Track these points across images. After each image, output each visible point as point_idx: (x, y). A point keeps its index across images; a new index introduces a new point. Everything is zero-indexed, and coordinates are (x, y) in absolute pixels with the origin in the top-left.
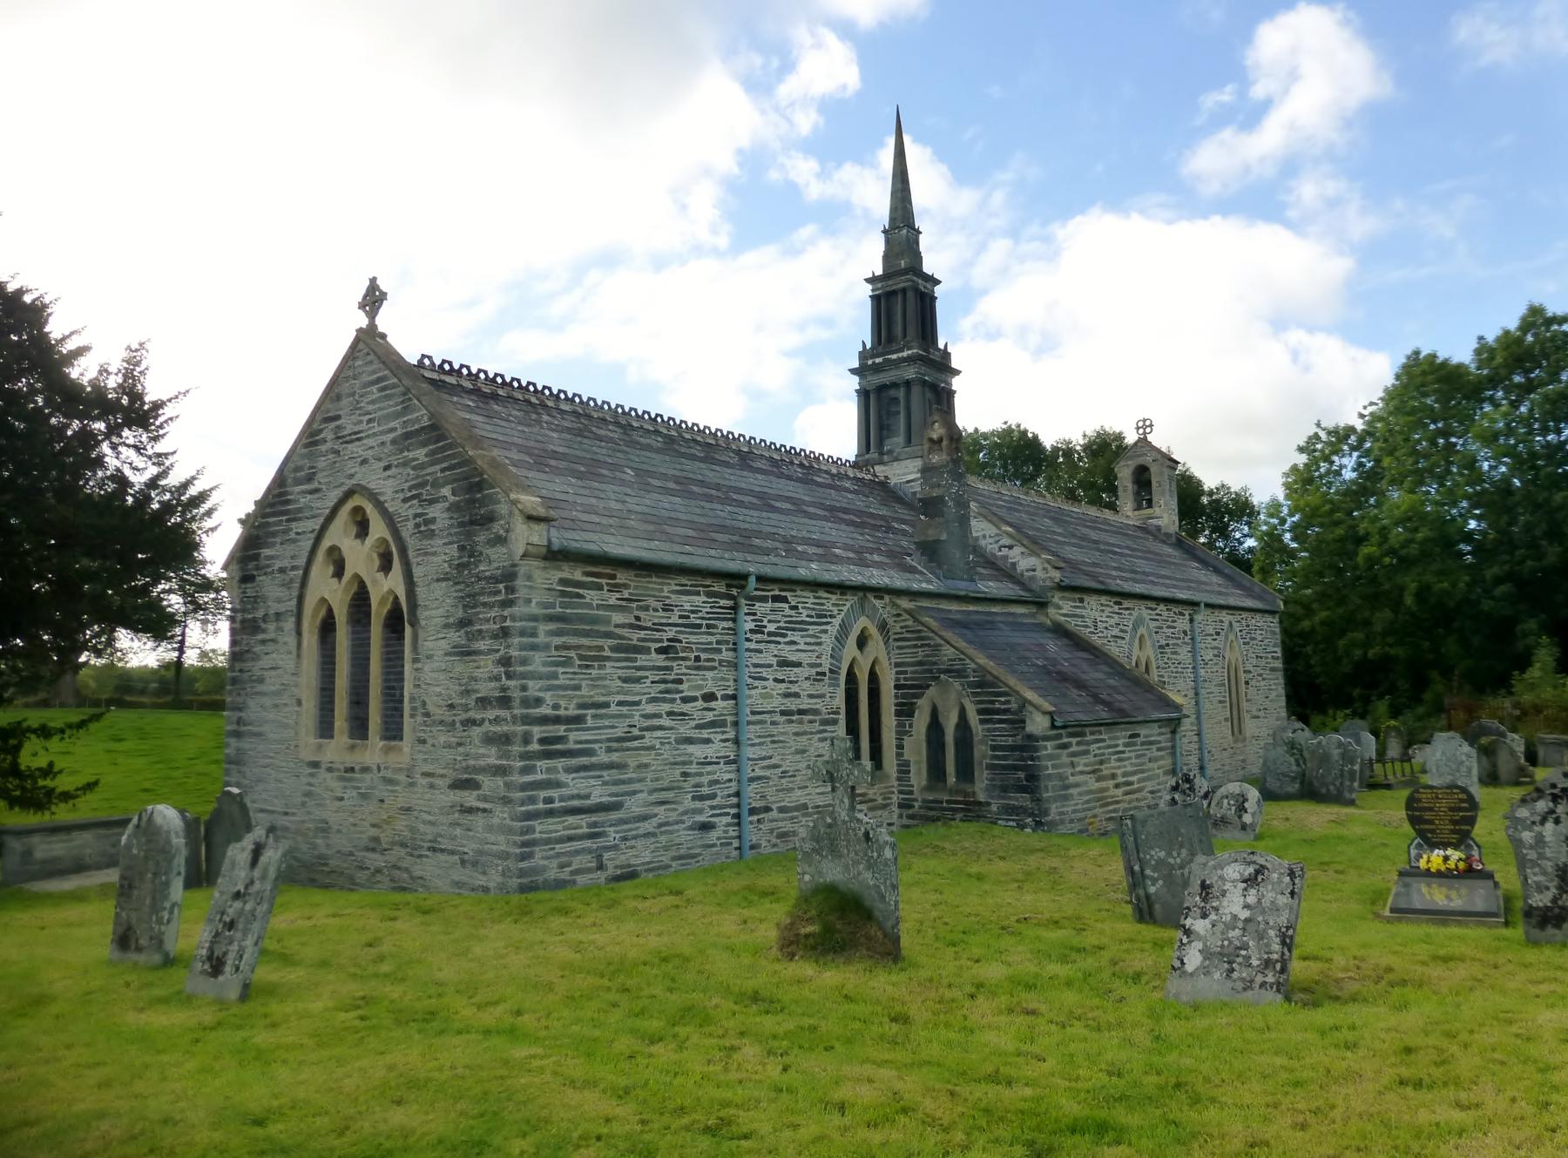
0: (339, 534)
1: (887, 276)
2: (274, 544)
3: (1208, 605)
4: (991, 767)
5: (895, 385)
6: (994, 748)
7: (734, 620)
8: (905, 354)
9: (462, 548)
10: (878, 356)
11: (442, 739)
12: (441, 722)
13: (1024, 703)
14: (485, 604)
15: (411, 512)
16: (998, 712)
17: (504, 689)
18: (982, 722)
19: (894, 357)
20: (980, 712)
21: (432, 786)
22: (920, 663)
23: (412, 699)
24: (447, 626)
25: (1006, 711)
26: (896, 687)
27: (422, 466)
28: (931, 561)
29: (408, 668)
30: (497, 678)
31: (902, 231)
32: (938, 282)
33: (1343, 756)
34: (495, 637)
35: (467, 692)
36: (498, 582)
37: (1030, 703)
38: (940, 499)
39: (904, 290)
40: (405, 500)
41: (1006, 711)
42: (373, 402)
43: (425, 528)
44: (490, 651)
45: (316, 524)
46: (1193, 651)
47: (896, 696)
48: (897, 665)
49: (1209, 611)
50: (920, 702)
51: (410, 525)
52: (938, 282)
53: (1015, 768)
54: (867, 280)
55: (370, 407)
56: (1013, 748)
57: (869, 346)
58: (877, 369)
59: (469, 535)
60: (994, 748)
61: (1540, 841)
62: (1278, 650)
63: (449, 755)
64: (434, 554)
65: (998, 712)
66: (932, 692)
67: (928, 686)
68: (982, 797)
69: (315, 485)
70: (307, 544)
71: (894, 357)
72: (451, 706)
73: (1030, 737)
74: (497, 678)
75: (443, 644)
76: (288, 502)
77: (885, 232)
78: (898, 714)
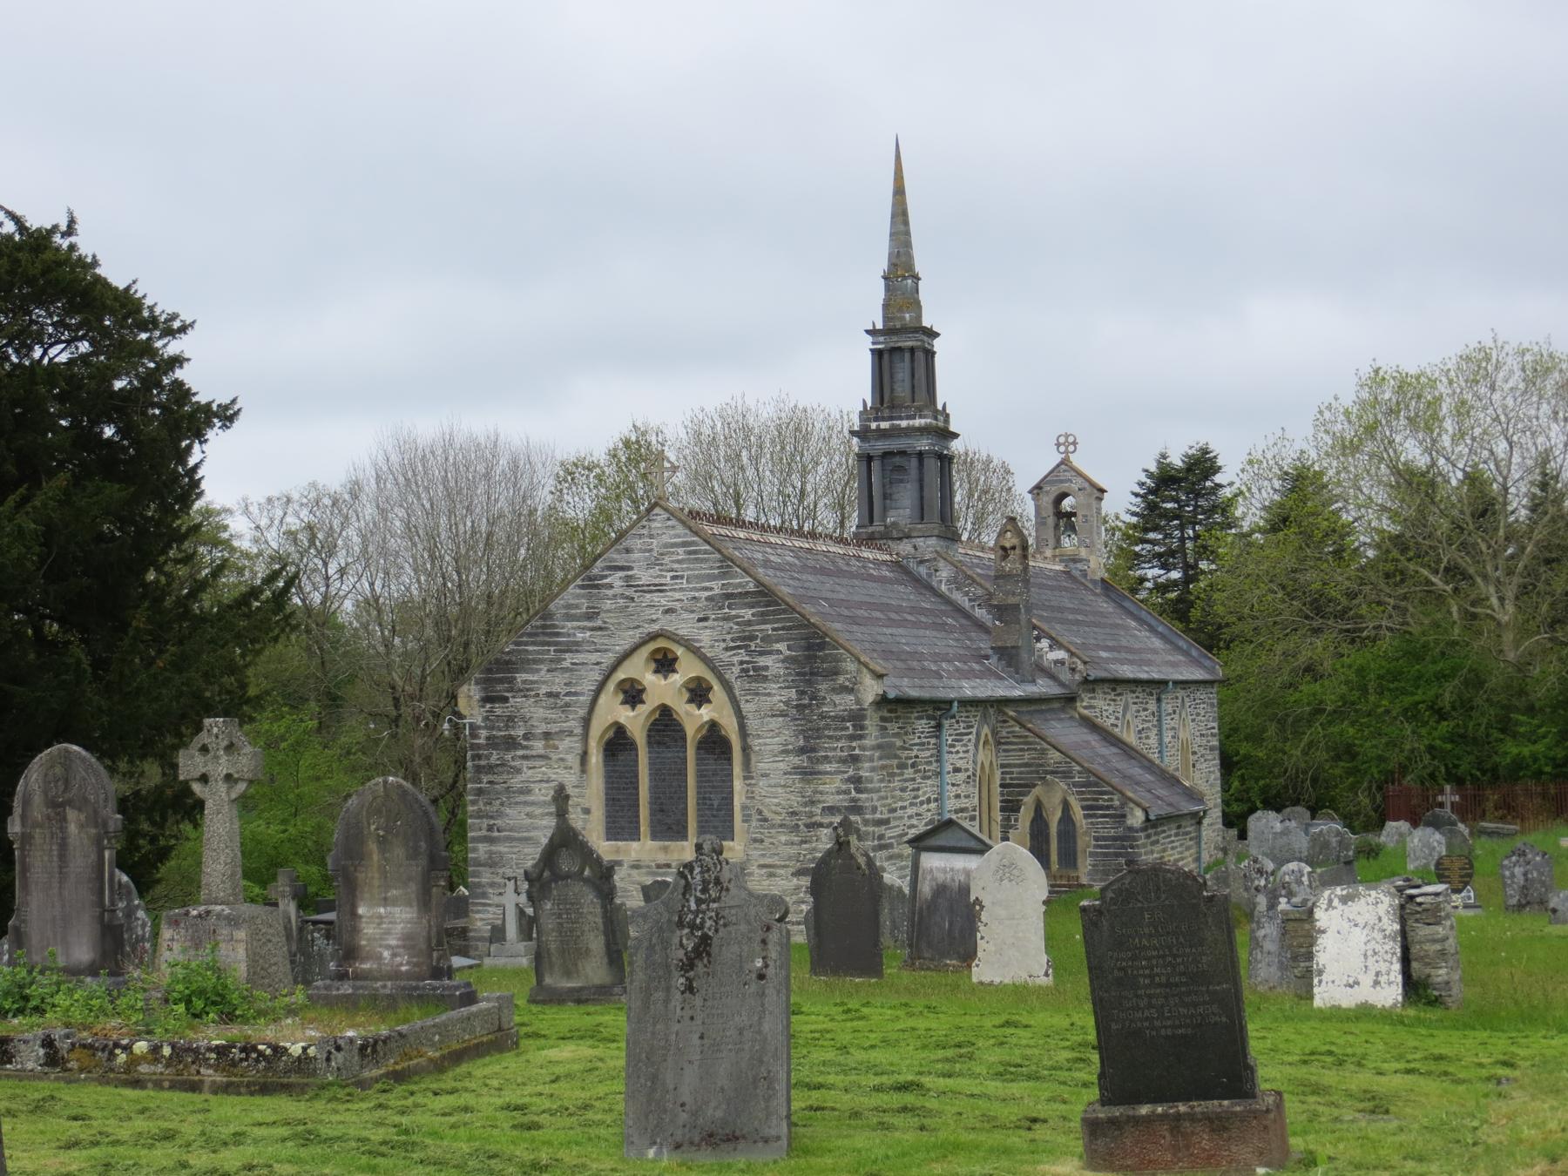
0: (639, 669)
1: (888, 331)
2: (538, 671)
3: (1176, 683)
4: (1091, 854)
5: (903, 453)
6: (1097, 839)
7: (937, 737)
8: (918, 422)
9: (801, 693)
10: (884, 419)
11: (783, 838)
12: (781, 826)
13: (1126, 800)
14: (830, 737)
15: (736, 659)
16: (1101, 808)
17: (853, 800)
18: (1086, 816)
19: (904, 423)
20: (1083, 808)
21: (771, 875)
22: (1026, 765)
23: (744, 807)
24: (783, 752)
25: (1108, 808)
26: (1002, 786)
27: (749, 623)
28: (1009, 665)
29: (738, 784)
30: (847, 792)
31: (901, 278)
32: (937, 335)
33: (1340, 843)
34: (843, 761)
35: (813, 803)
36: (843, 720)
37: (1131, 800)
38: (1016, 607)
39: (912, 350)
40: (727, 649)
41: (1108, 808)
42: (679, 562)
43: (756, 675)
44: (838, 772)
45: (608, 659)
46: (1160, 734)
47: (1002, 794)
48: (1002, 766)
49: (1181, 693)
50: (1026, 799)
51: (736, 670)
52: (937, 335)
53: (1117, 855)
54: (867, 332)
55: (676, 566)
56: (1115, 839)
57: (869, 404)
58: (882, 434)
59: (809, 683)
60: (1097, 839)
61: (1513, 875)
62: (1215, 725)
63: (793, 850)
64: (769, 695)
65: (1101, 808)
66: (1036, 791)
67: (1034, 786)
68: (1084, 880)
69: (599, 623)
70: (597, 676)
71: (904, 423)
72: (794, 813)
73: (1131, 829)
74: (847, 792)
75: (782, 765)
76: (558, 634)
77: (885, 278)
78: (1003, 809)
